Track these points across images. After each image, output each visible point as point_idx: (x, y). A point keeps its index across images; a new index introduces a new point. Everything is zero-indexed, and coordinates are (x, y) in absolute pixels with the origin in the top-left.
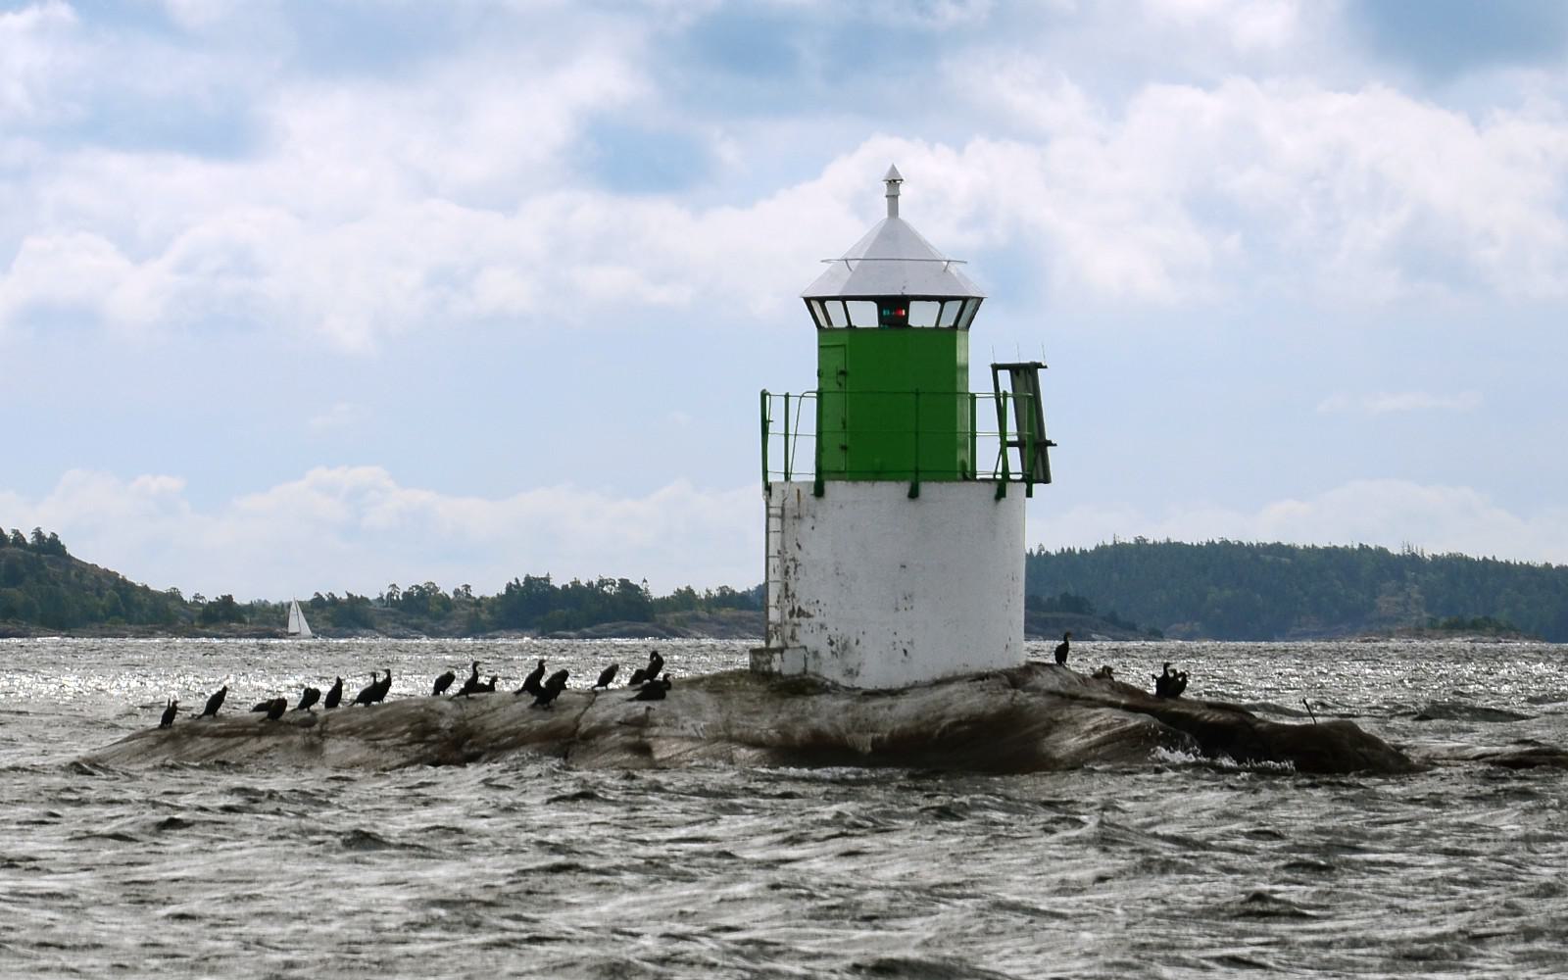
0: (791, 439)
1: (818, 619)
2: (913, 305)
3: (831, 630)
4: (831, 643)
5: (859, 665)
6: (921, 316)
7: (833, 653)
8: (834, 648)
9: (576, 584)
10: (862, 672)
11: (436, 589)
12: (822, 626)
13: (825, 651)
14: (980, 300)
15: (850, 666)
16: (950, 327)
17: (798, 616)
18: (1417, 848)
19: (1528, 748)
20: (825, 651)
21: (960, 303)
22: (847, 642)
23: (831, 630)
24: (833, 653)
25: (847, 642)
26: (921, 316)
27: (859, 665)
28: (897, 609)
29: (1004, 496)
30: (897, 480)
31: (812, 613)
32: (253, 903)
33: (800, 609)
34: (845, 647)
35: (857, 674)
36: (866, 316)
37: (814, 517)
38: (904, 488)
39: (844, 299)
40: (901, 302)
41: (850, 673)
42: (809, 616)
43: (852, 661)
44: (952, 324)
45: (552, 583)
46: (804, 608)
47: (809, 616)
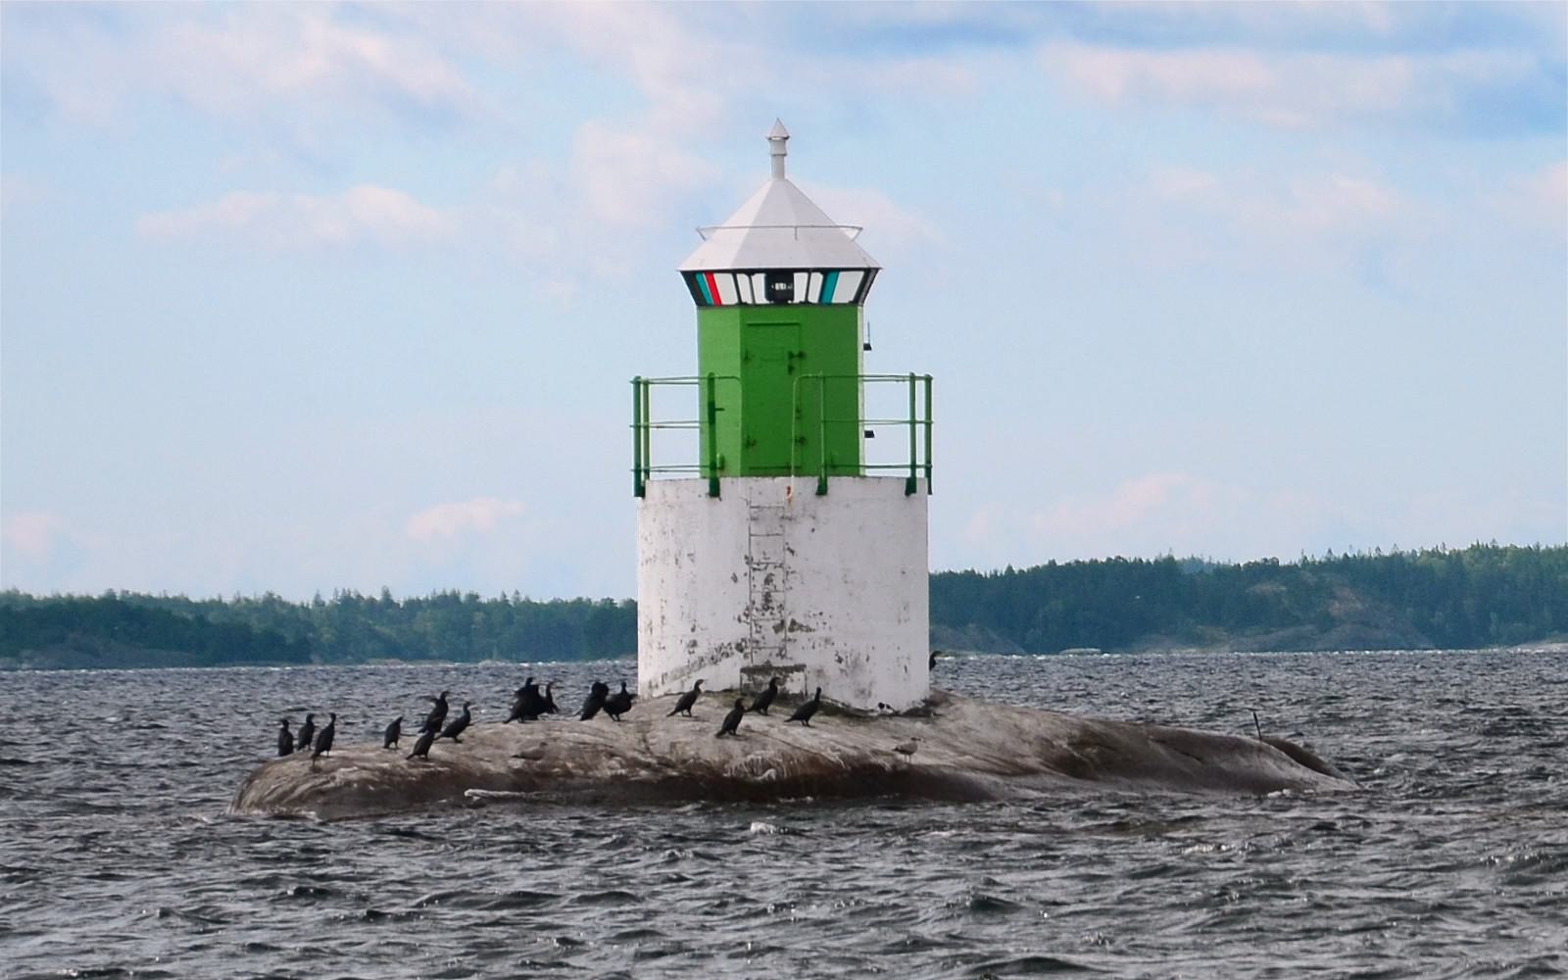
0: (921, 416)
1: (822, 633)
2: (796, 275)
3: (839, 645)
4: (840, 660)
5: (871, 684)
6: (805, 289)
7: (842, 670)
8: (843, 665)
9: (1052, 563)
10: (874, 691)
11: (1096, 561)
12: (827, 641)
13: (832, 669)
14: (877, 270)
15: (861, 687)
16: (851, 302)
17: (791, 630)
18: (63, 947)
19: (792, 814)
20: (832, 669)
21: (862, 274)
22: (856, 659)
23: (839, 645)
24: (842, 670)
25: (856, 659)
26: (805, 289)
27: (871, 684)
28: (899, 621)
29: (914, 491)
30: (813, 476)
31: (812, 627)
32: (258, 957)
33: (793, 622)
34: (856, 664)
35: (870, 694)
36: (756, 291)
37: (814, 518)
38: (812, 483)
39: (734, 272)
40: (786, 275)
41: (862, 693)
42: (809, 630)
43: (864, 680)
44: (852, 299)
45: (224, 600)
46: (800, 620)
47: (809, 630)
